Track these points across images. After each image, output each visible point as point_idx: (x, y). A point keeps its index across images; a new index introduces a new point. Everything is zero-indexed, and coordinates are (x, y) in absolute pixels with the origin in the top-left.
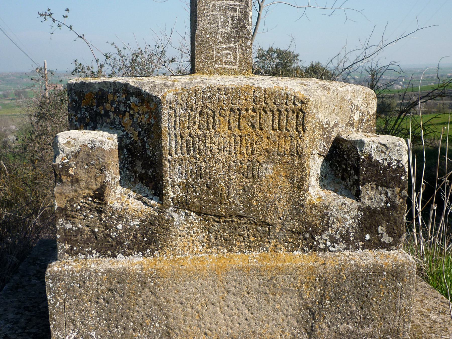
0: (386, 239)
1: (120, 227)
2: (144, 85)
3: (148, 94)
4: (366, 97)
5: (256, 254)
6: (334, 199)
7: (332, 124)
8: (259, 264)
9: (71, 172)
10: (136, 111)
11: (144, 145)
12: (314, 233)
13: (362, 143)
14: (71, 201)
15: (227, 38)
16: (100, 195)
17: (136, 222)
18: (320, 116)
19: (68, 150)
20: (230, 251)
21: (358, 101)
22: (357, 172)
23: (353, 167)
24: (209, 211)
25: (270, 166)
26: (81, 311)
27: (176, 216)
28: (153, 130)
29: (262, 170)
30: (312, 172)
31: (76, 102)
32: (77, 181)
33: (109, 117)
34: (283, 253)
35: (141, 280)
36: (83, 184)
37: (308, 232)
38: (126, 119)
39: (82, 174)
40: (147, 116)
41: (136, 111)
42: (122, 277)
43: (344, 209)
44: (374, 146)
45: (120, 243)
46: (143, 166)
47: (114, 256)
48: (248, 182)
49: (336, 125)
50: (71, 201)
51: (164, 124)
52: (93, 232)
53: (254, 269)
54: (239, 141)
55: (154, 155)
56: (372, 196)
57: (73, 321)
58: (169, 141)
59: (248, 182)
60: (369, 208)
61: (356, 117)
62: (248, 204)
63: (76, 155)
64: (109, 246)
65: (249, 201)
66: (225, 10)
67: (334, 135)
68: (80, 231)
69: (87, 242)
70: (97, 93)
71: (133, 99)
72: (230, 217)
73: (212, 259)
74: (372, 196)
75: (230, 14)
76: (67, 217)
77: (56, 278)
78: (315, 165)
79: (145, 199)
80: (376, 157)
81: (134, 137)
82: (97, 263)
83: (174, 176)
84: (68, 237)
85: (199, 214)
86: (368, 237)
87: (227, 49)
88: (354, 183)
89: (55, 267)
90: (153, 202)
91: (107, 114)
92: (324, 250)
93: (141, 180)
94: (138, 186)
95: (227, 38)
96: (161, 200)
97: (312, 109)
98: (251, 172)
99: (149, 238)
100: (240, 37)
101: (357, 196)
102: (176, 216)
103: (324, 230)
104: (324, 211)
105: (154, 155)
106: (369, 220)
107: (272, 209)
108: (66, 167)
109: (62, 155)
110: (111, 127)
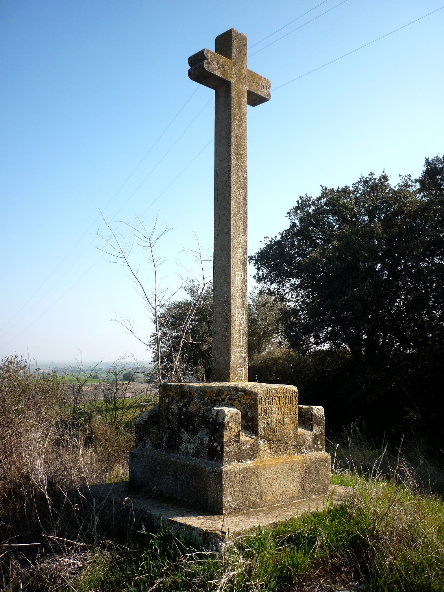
0: (320, 447)
1: (244, 448)
3: (250, 391)
10: (243, 398)
15: (240, 366)
19: (229, 415)
20: (277, 456)
23: (309, 418)
24: (271, 439)
25: (288, 419)
26: (234, 488)
27: (261, 442)
31: (201, 395)
33: (224, 401)
36: (233, 430)
40: (249, 400)
41: (243, 398)
42: (247, 470)
45: (244, 456)
47: (242, 462)
52: (235, 451)
55: (252, 417)
64: (240, 458)
65: (282, 433)
66: (240, 353)
68: (231, 451)
70: (216, 391)
75: (241, 355)
77: (226, 474)
79: (250, 436)
85: (267, 441)
87: (240, 370)
88: (309, 425)
90: (253, 437)
91: (223, 400)
98: (283, 422)
101: (311, 430)
102: (261, 442)
105: (252, 417)
108: (228, 422)
109: (227, 418)
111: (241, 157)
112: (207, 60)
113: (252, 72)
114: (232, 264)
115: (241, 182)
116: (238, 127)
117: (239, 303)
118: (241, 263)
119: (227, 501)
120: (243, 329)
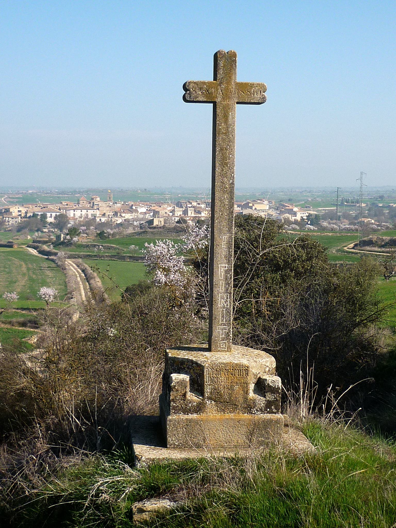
0: (274, 410)
1: (190, 405)
2: (199, 361)
4: (271, 362)
5: (232, 414)
6: (257, 397)
7: (258, 373)
8: (233, 418)
9: (176, 388)
11: (198, 379)
12: (251, 408)
13: (266, 380)
14: (176, 397)
15: (223, 339)
16: (185, 395)
17: (195, 404)
18: (253, 371)
19: (175, 381)
20: (224, 413)
21: (268, 364)
22: (265, 389)
27: (207, 402)
28: (201, 375)
29: (235, 388)
30: (250, 389)
32: (178, 391)
34: (241, 414)
35: (196, 422)
36: (179, 392)
37: (249, 407)
38: (192, 371)
39: (179, 389)
42: (190, 421)
43: (261, 401)
44: (270, 381)
45: (190, 410)
46: (197, 386)
47: (188, 414)
48: (230, 392)
49: (259, 373)
50: (176, 397)
51: (205, 374)
53: (232, 419)
54: (228, 379)
56: (270, 397)
57: (175, 435)
58: (206, 378)
59: (230, 392)
60: (268, 400)
61: (267, 369)
62: (230, 398)
63: (178, 382)
64: (186, 411)
67: (258, 376)
68: (178, 406)
69: (180, 410)
71: (194, 365)
72: (225, 403)
73: (218, 416)
74: (270, 397)
75: (224, 331)
76: (174, 402)
77: (170, 421)
78: (252, 387)
80: (270, 384)
81: (194, 377)
82: (183, 417)
83: (208, 390)
84: (174, 408)
85: (215, 401)
86: (268, 410)
89: (170, 417)
90: (201, 397)
91: (184, 368)
92: (254, 414)
93: (196, 390)
94: (195, 392)
95: (223, 339)
96: (203, 397)
97: (250, 369)
98: (231, 388)
99: (199, 408)
100: (228, 339)
101: (265, 397)
102: (207, 402)
103: (254, 407)
104: (254, 401)
106: (269, 404)
107: (237, 400)
108: (175, 386)
110: (186, 373)
111: (227, 166)
112: (189, 91)
113: (242, 84)
114: (215, 259)
115: (226, 188)
116: (223, 140)
117: (222, 290)
118: (225, 257)
119: (170, 439)
120: (226, 310)
